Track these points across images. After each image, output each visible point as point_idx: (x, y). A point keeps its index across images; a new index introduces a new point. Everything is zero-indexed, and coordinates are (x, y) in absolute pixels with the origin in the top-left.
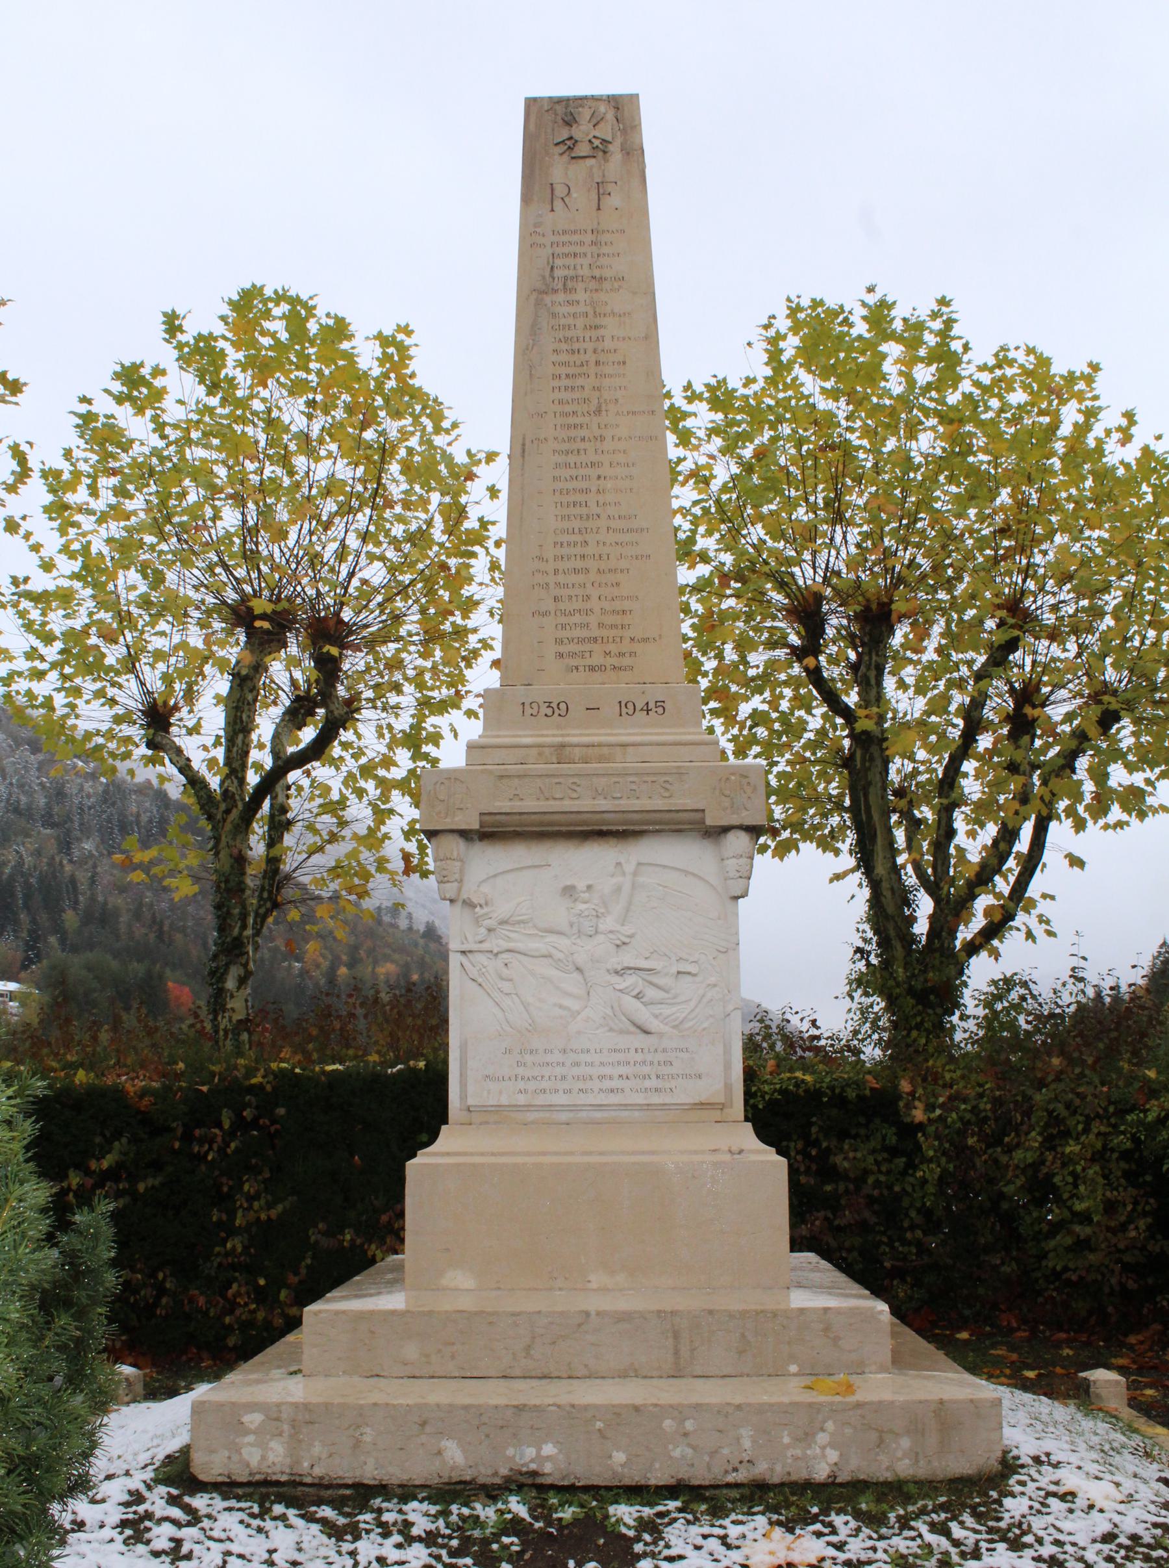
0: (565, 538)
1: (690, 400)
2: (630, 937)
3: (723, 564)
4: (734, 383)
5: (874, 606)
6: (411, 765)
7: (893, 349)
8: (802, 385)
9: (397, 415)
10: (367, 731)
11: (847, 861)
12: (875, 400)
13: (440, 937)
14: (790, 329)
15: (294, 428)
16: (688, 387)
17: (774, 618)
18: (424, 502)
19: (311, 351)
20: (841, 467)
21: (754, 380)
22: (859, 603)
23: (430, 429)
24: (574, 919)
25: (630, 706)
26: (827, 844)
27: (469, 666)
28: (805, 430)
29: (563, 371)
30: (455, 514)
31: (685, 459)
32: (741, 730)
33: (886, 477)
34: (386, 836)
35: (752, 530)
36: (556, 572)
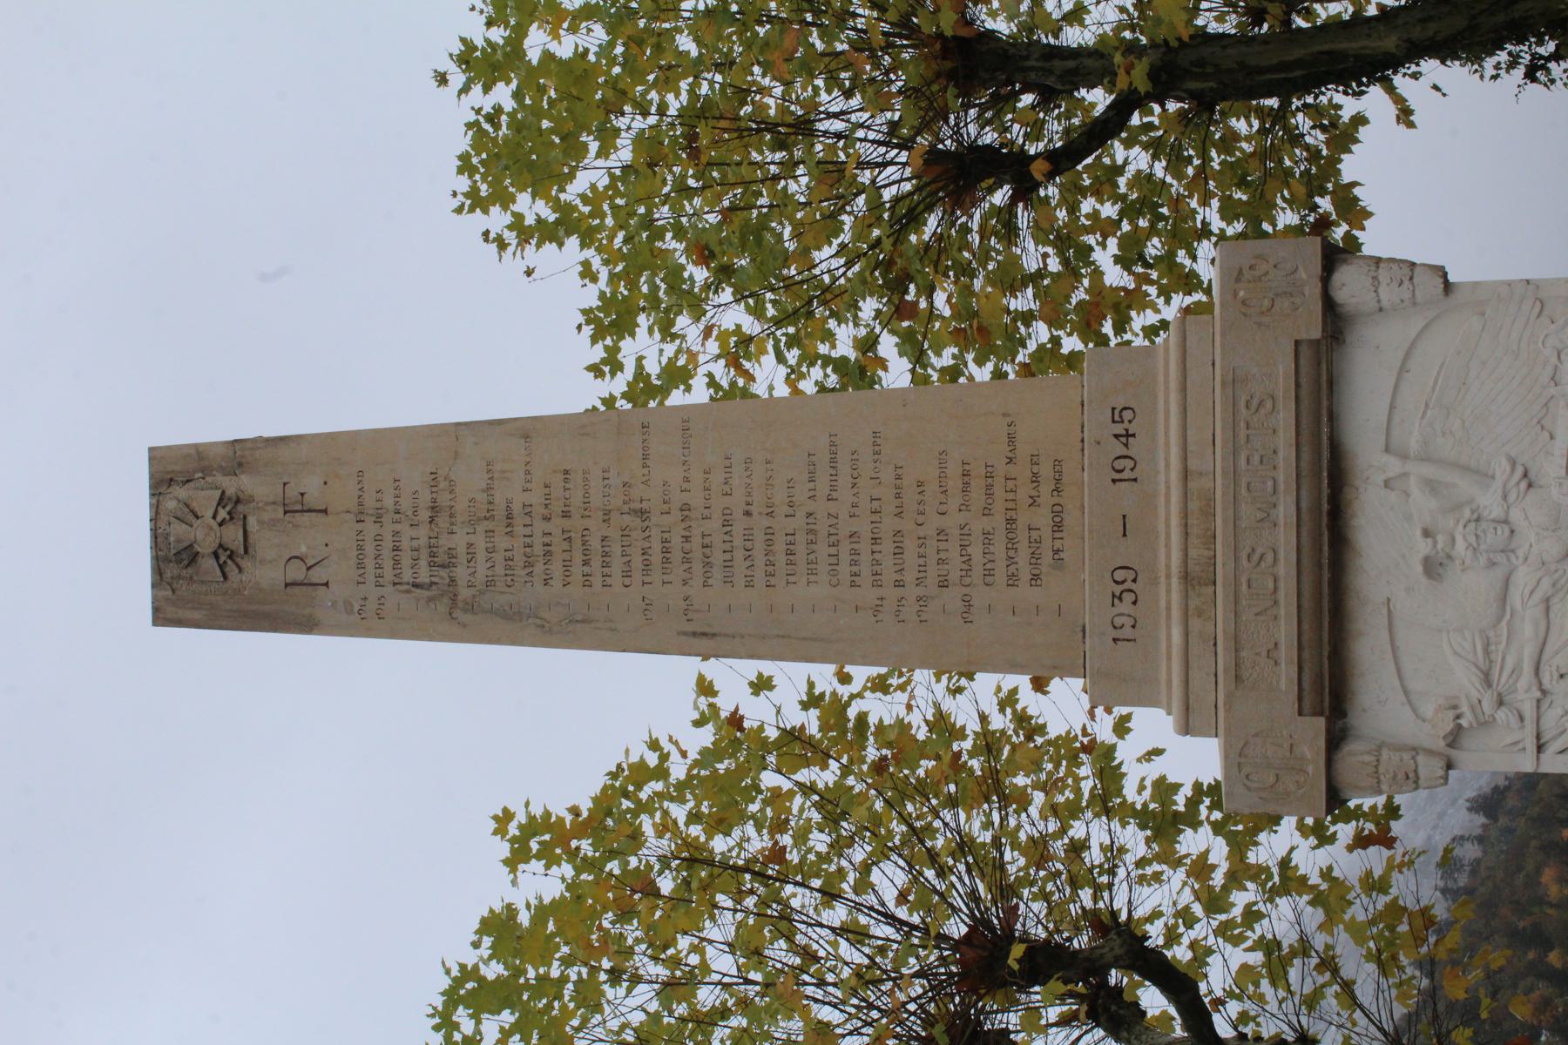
0: (845, 569)
1: (617, 367)
2: (1513, 464)
3: (878, 312)
4: (590, 296)
5: (948, 65)
6: (1206, 830)
7: (536, 42)
8: (593, 187)
9: (636, 839)
10: (1149, 899)
11: (1374, 101)
12: (617, 70)
13: (1496, 788)
14: (505, 207)
15: (653, 1006)
16: (596, 370)
17: (965, 230)
18: (776, 796)
19: (531, 973)
20: (723, 124)
21: (586, 264)
22: (944, 90)
23: (658, 786)
24: (1483, 560)
25: (1119, 464)
26: (1344, 136)
27: (1041, 730)
28: (664, 182)
29: (577, 570)
30: (795, 747)
31: (710, 375)
32: (1151, 282)
33: (738, 49)
34: (1326, 874)
35: (824, 266)
36: (899, 584)
